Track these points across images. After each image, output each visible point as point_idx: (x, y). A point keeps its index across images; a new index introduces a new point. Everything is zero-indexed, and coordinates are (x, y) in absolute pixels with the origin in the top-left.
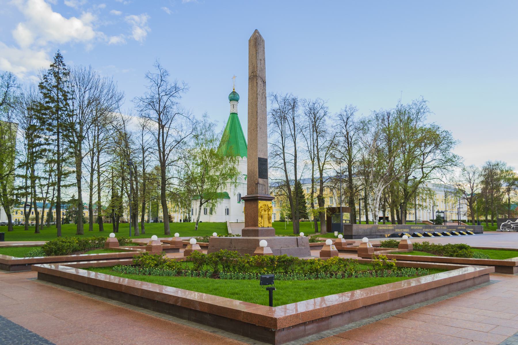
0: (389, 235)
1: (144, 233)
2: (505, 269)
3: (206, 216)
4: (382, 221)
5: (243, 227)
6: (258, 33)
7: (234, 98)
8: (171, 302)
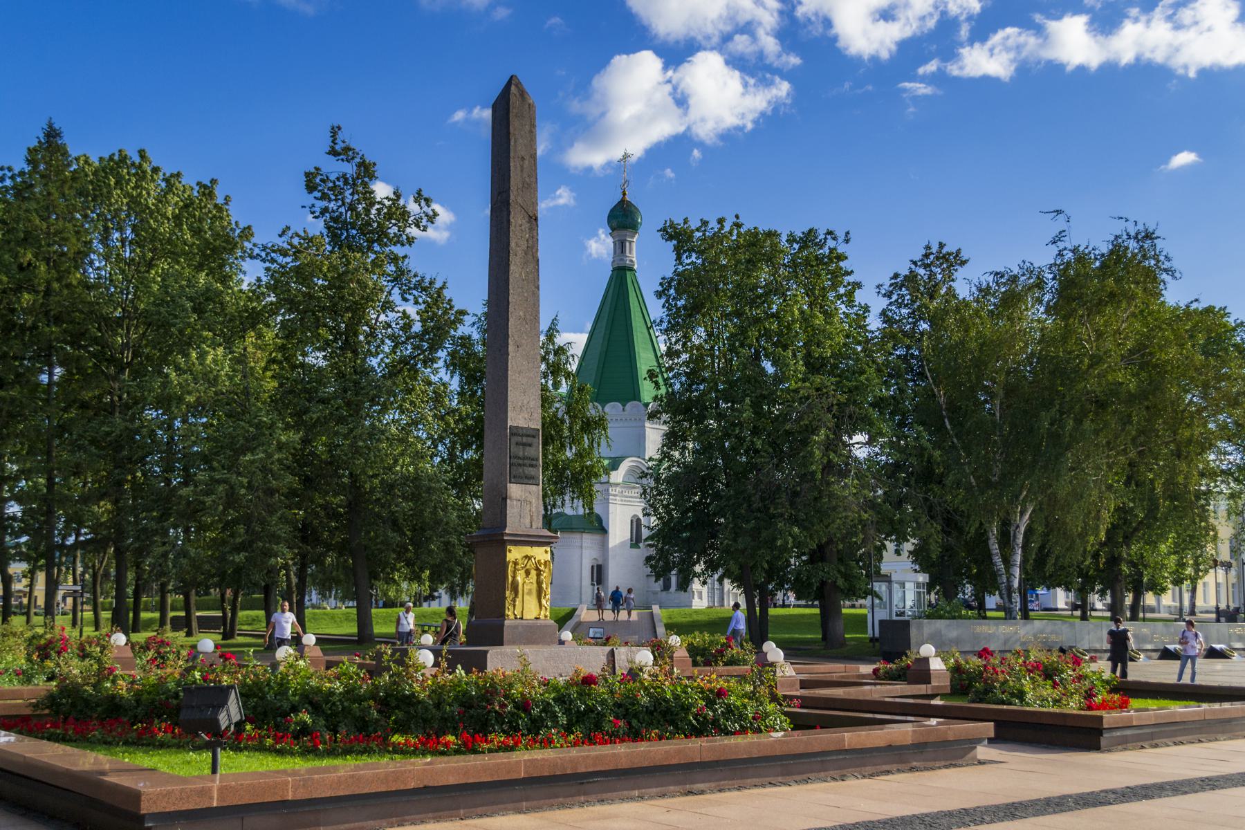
6: (518, 85)
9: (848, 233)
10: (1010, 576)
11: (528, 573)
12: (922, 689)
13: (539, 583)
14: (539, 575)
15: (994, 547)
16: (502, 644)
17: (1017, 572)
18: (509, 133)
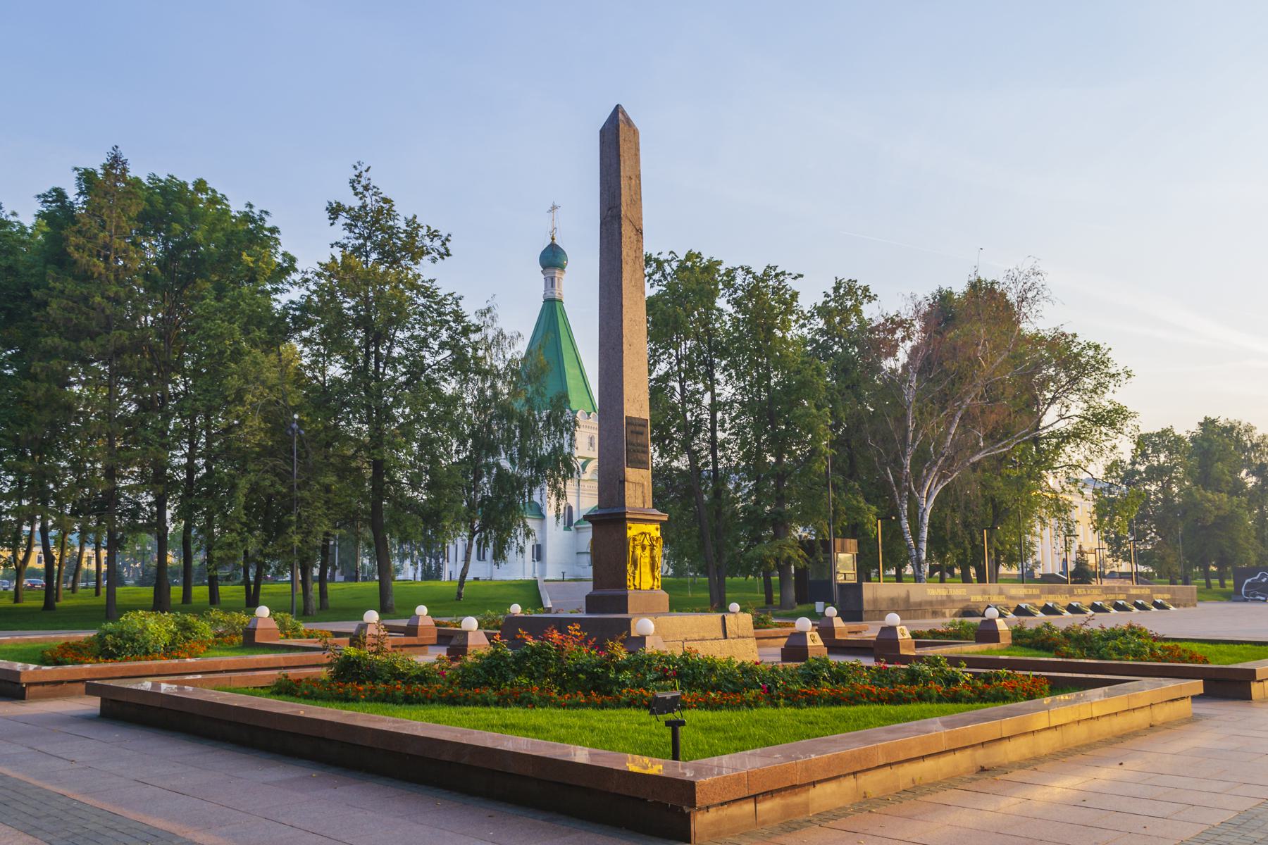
0: (954, 611)
1: (327, 608)
2: (1229, 686)
3: (482, 564)
4: (937, 574)
5: (588, 588)
6: (623, 112)
7: (552, 259)
8: (445, 757)
9: (801, 276)
10: (918, 549)
11: (644, 548)
12: (994, 646)
13: (653, 558)
14: (652, 550)
15: (905, 524)
16: (861, 620)
17: (924, 546)
18: (619, 156)
